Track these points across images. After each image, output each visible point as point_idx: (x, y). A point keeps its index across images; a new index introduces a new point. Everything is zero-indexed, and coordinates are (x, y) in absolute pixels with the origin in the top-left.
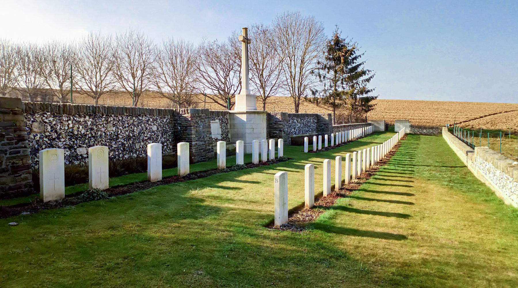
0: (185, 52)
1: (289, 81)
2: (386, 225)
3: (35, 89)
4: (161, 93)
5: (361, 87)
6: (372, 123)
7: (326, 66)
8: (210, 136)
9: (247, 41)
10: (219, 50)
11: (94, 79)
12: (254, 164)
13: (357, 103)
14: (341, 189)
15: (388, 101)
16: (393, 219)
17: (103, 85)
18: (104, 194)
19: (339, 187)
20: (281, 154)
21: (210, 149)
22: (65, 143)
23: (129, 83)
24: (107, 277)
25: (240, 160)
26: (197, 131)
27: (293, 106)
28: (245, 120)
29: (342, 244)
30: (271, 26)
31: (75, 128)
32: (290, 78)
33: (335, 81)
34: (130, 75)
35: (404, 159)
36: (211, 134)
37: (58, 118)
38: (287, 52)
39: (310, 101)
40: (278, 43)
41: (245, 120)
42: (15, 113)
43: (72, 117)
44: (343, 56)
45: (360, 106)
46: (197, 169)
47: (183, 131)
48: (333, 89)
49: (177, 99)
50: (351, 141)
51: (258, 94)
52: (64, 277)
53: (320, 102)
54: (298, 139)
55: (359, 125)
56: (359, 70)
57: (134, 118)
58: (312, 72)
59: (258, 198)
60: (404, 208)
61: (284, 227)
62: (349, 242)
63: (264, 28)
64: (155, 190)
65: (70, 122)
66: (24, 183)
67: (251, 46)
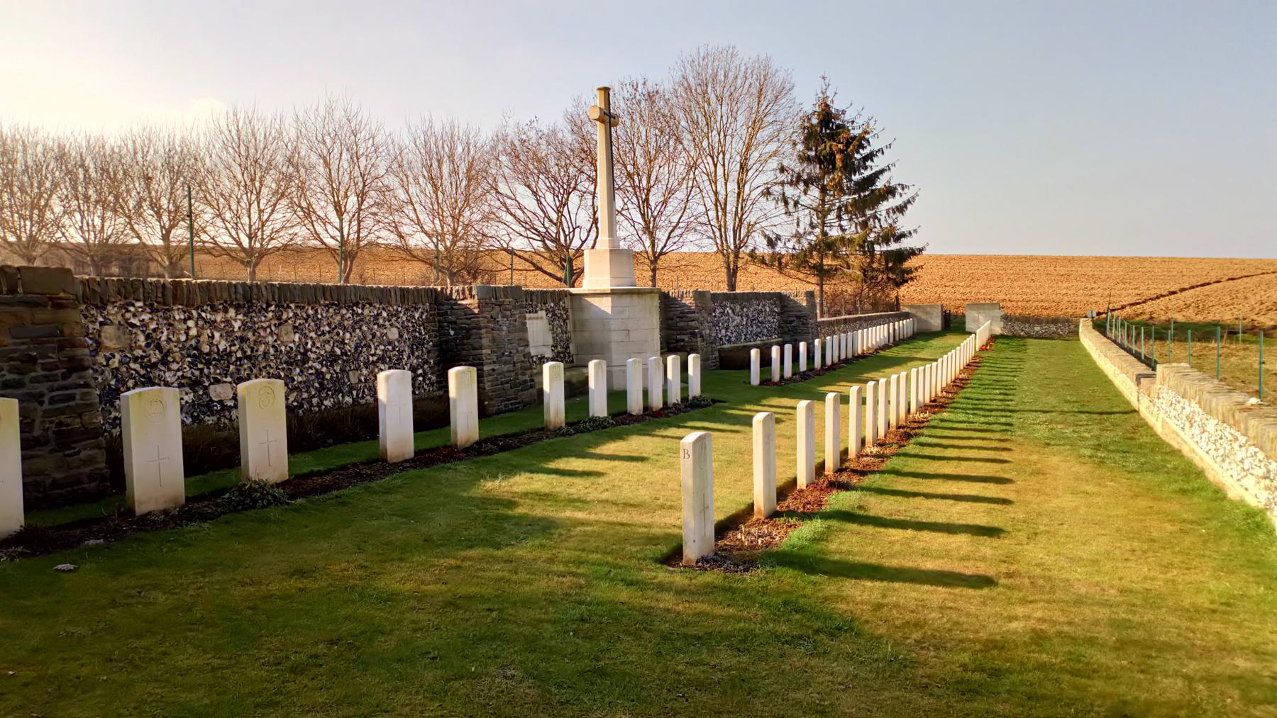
0: (460, 149)
1: (712, 214)
2: (947, 554)
4: (407, 250)
7: (799, 177)
8: (527, 350)
9: (608, 118)
10: (543, 142)
11: (245, 220)
12: (631, 415)
13: (875, 266)
14: (840, 471)
15: (948, 259)
16: (962, 539)
17: (267, 233)
19: (835, 465)
20: (695, 389)
21: (525, 382)
22: (180, 374)
23: (329, 227)
24: (291, 686)
25: (598, 406)
26: (494, 340)
27: (723, 275)
28: (609, 311)
29: (844, 599)
31: (204, 338)
32: (713, 207)
33: (822, 212)
34: (331, 208)
36: (527, 345)
37: (161, 314)
38: (705, 144)
39: (763, 261)
40: (683, 123)
41: (609, 311)
43: (194, 312)
44: (841, 151)
46: (497, 430)
47: (461, 339)
48: (817, 231)
50: (863, 356)
53: (787, 265)
54: (735, 352)
55: (881, 317)
56: (880, 184)
57: (344, 311)
58: (767, 193)
59: (643, 494)
60: (989, 513)
61: (705, 562)
62: (860, 595)
63: (651, 86)
64: (399, 482)
65: (191, 323)
66: (87, 470)
67: (619, 131)
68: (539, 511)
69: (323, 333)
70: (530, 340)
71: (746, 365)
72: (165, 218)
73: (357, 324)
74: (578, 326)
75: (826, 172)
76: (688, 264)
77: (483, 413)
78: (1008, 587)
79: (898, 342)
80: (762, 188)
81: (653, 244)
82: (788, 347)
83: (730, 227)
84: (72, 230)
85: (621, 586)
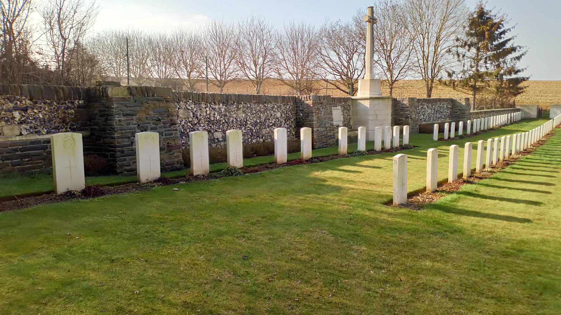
0: (306, 36)
1: (421, 62)
2: (513, 210)
3: (166, 78)
4: (282, 80)
6: (522, 108)
8: (332, 122)
9: (372, 20)
10: (342, 31)
11: (219, 68)
13: (503, 86)
15: (545, 83)
16: (522, 205)
17: (227, 74)
18: (240, 171)
19: (468, 174)
20: (406, 141)
21: (331, 135)
24: (251, 228)
25: (362, 146)
26: (318, 118)
28: (368, 106)
29: (459, 222)
31: (212, 115)
32: (422, 58)
33: (477, 60)
34: (252, 63)
35: (554, 149)
39: (445, 84)
40: (409, 19)
41: (368, 106)
42: (168, 101)
44: (488, 30)
45: (507, 89)
46: (319, 154)
47: (305, 117)
48: (474, 69)
50: (493, 129)
51: (385, 78)
52: (220, 226)
54: (424, 124)
55: (504, 110)
56: (508, 46)
57: (261, 105)
58: (449, 51)
59: (378, 180)
61: (402, 205)
62: (466, 221)
63: (394, 3)
64: (282, 170)
65: (208, 109)
66: (176, 160)
68: (335, 184)
69: (253, 114)
70: (334, 118)
71: (432, 132)
72: (189, 68)
75: (480, 40)
76: (409, 85)
77: (246, 156)
78: (537, 224)
79: (512, 122)
80: (447, 49)
81: (392, 76)
83: (430, 68)
84: (154, 73)
85: (366, 210)
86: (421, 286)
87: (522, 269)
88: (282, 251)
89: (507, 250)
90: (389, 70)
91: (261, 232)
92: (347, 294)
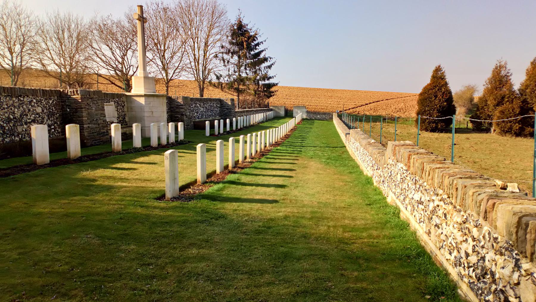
0: (73, 26)
1: (193, 64)
2: (265, 194)
4: (47, 72)
5: (263, 73)
7: (229, 51)
8: (104, 118)
9: (142, 19)
10: (114, 25)
12: (152, 147)
14: (234, 167)
15: (289, 88)
16: (272, 189)
19: (232, 165)
20: (181, 137)
21: (104, 132)
23: (6, 59)
25: (137, 142)
26: (88, 114)
27: (198, 91)
30: (171, 4)
32: (193, 61)
33: (239, 66)
34: (7, 50)
36: (105, 117)
38: (189, 33)
40: (180, 23)
44: (246, 41)
47: (73, 113)
48: (237, 74)
49: (67, 79)
51: (160, 76)
53: (224, 87)
56: (262, 56)
57: (14, 99)
58: (216, 56)
59: (153, 176)
60: (284, 180)
61: (174, 199)
63: (165, 5)
64: (42, 172)
67: (146, 25)
68: (106, 183)
69: (4, 109)
70: (106, 114)
71: (204, 128)
73: (22, 104)
74: (129, 110)
76: (182, 85)
77: (83, 145)
79: (267, 120)
82: (222, 121)
83: (201, 70)
85: (138, 207)
86: (187, 274)
87: (270, 243)
88: (35, 264)
89: (260, 228)
90: (164, 68)
91: (8, 247)
92: (110, 299)
